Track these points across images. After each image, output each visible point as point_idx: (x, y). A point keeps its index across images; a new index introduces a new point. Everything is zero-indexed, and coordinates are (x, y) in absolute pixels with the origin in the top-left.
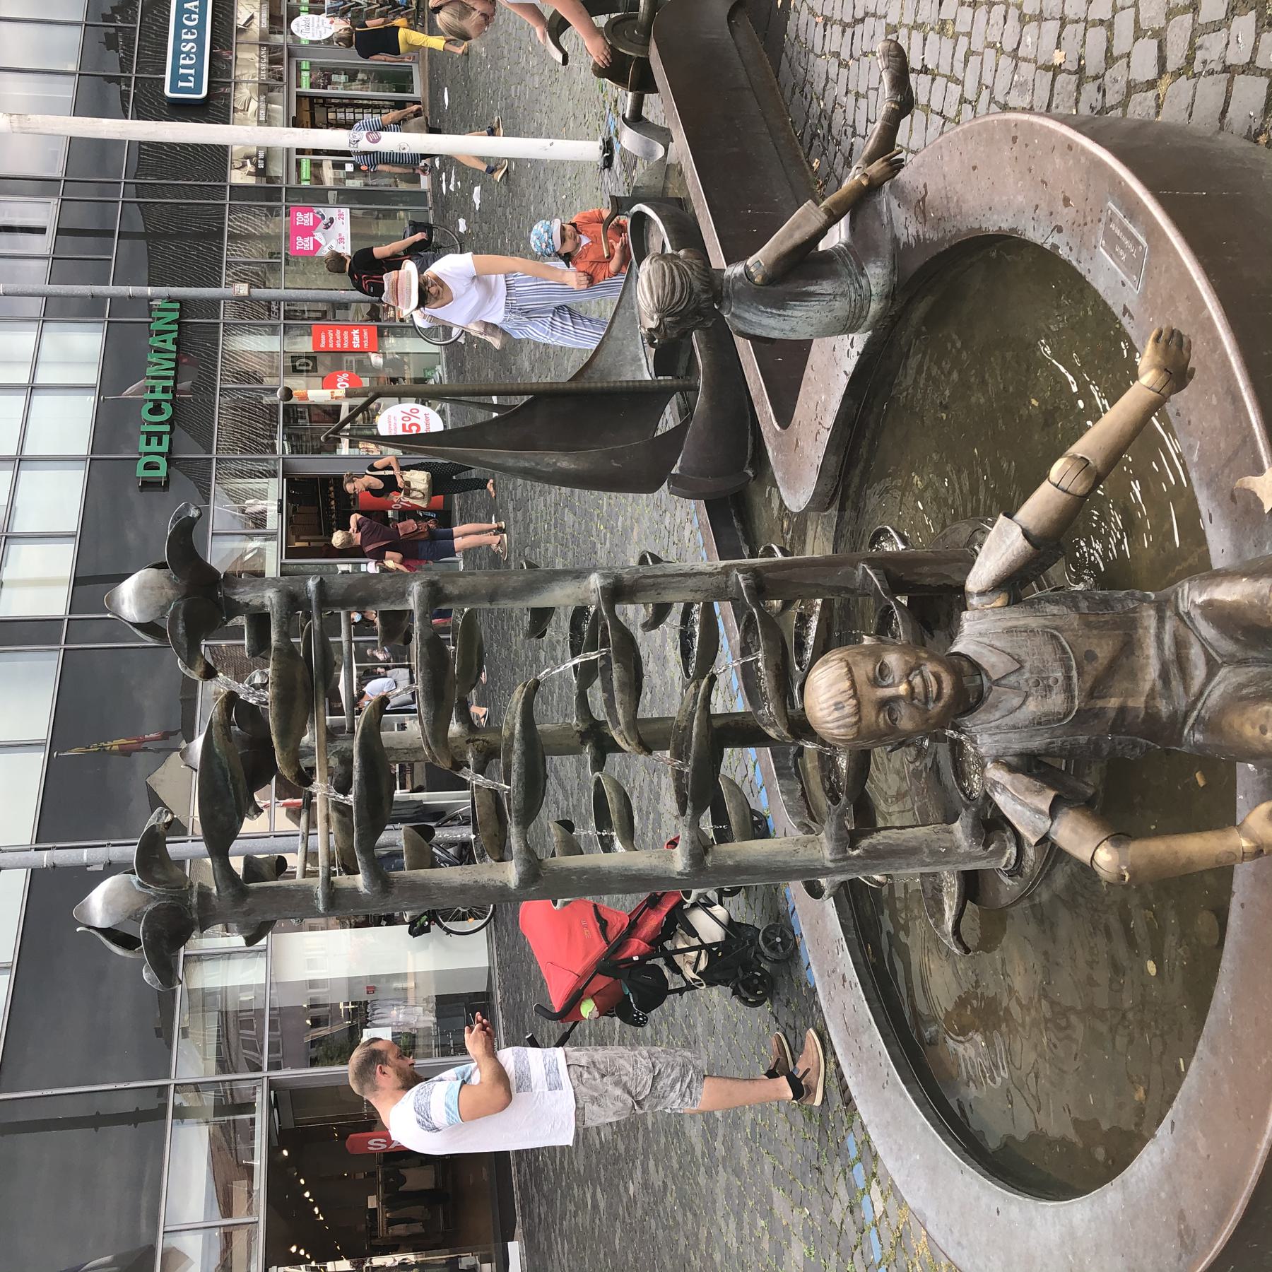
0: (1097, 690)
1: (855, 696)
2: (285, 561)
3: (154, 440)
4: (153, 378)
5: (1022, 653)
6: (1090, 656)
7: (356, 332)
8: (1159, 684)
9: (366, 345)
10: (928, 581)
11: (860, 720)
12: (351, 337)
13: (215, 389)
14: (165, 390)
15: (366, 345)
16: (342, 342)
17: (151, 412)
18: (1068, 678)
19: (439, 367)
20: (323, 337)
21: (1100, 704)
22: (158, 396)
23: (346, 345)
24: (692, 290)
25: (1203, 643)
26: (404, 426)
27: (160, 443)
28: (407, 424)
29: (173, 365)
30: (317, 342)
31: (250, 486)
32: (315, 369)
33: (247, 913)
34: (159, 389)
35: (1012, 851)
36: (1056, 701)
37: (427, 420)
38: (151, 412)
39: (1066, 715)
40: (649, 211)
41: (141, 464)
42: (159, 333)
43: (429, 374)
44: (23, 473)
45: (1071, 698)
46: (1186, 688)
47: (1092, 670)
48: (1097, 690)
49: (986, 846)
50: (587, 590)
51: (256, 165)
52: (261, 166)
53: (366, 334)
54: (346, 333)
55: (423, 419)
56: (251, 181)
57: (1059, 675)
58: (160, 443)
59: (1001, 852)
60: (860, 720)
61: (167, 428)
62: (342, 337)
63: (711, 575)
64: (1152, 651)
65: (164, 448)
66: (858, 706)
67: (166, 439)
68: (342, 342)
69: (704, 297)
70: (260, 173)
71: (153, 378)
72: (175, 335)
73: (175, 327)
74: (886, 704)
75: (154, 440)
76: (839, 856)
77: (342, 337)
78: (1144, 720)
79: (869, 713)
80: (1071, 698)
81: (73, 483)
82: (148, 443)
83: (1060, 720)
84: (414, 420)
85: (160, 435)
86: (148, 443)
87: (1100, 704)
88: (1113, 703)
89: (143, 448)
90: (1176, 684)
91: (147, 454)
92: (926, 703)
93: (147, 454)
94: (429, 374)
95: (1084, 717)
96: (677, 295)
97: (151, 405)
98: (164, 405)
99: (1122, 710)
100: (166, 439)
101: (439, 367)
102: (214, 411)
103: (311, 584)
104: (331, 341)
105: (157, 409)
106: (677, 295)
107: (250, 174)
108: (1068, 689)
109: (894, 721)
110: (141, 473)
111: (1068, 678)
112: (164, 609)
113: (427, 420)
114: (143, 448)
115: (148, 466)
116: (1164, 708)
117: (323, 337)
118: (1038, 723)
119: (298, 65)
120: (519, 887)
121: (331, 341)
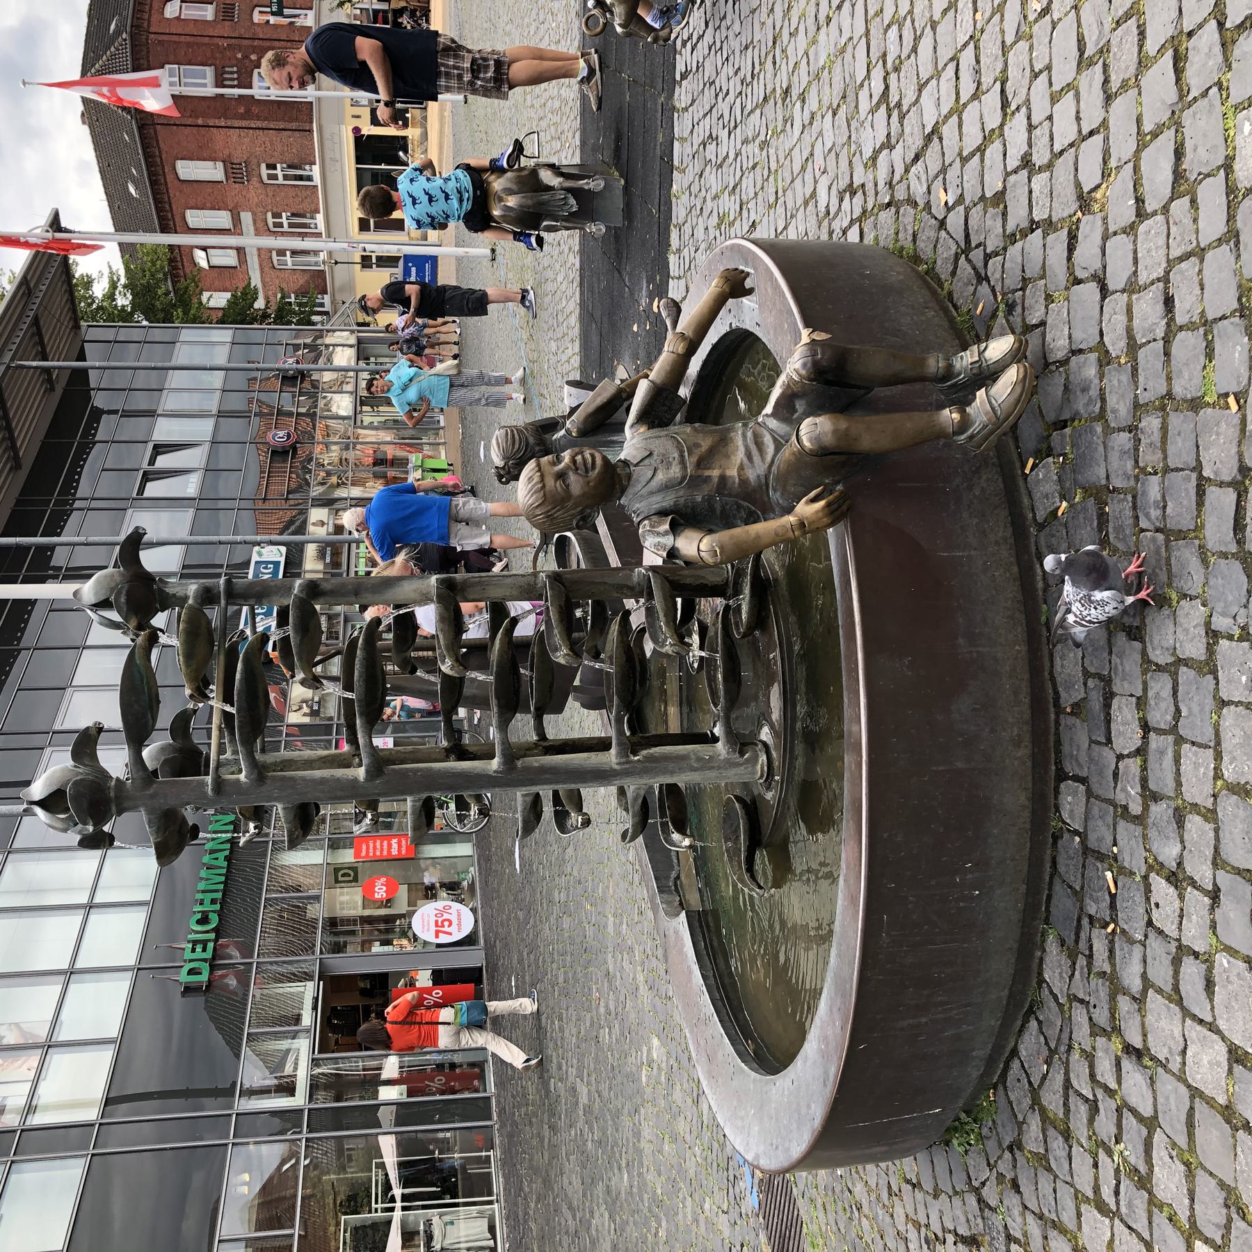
0: (703, 463)
1: (540, 470)
2: (317, 1055)
3: (199, 948)
4: (203, 892)
5: (652, 447)
6: (697, 445)
7: (394, 841)
8: (746, 461)
9: (404, 852)
10: (688, 581)
11: (544, 486)
12: (390, 846)
13: (260, 898)
14: (213, 901)
15: (404, 852)
16: (382, 850)
17: (198, 922)
18: (682, 456)
19: (472, 869)
20: (364, 847)
21: (707, 473)
22: (207, 907)
23: (385, 853)
24: (527, 444)
25: (771, 431)
26: (437, 922)
27: (204, 950)
28: (440, 920)
29: (223, 879)
30: (357, 855)
31: (292, 990)
32: (356, 880)
33: (152, 797)
34: (207, 902)
35: (763, 758)
36: (675, 471)
37: (459, 915)
38: (198, 922)
39: (684, 478)
40: (573, 538)
41: (185, 970)
42: (212, 852)
43: (463, 876)
44: (72, 987)
45: (684, 467)
46: (763, 459)
47: (698, 452)
48: (703, 463)
49: (742, 754)
50: (428, 586)
51: (311, 707)
52: (316, 708)
53: (404, 842)
54: (385, 843)
55: (455, 914)
56: (307, 720)
57: (676, 455)
58: (204, 950)
59: (754, 759)
60: (544, 486)
61: (212, 936)
62: (382, 846)
63: (523, 576)
64: (740, 442)
65: (208, 954)
66: (542, 476)
67: (211, 945)
68: (382, 850)
69: (537, 448)
70: (314, 713)
71: (203, 892)
72: (227, 853)
73: (228, 846)
74: (561, 476)
75: (199, 948)
76: (623, 760)
77: (382, 846)
78: (740, 484)
79: (550, 482)
80: (684, 467)
81: (116, 992)
82: (193, 950)
83: (681, 483)
84: (446, 916)
85: (204, 943)
86: (193, 950)
87: (707, 473)
88: (715, 473)
89: (188, 955)
90: (756, 458)
91: (191, 961)
92: (587, 471)
93: (191, 961)
94: (463, 876)
95: (695, 481)
96: (517, 446)
97: (199, 916)
98: (211, 916)
99: (723, 478)
100: (211, 945)
101: (472, 869)
102: (257, 921)
103: (222, 581)
104: (371, 850)
105: (204, 920)
106: (517, 446)
107: (305, 715)
108: (682, 462)
109: (567, 486)
110: (183, 977)
111: (682, 456)
112: (112, 590)
113: (459, 915)
114: (188, 955)
115: (191, 972)
116: (751, 475)
117: (364, 847)
118: (666, 487)
119: (353, 627)
120: (366, 780)
121: (371, 850)
